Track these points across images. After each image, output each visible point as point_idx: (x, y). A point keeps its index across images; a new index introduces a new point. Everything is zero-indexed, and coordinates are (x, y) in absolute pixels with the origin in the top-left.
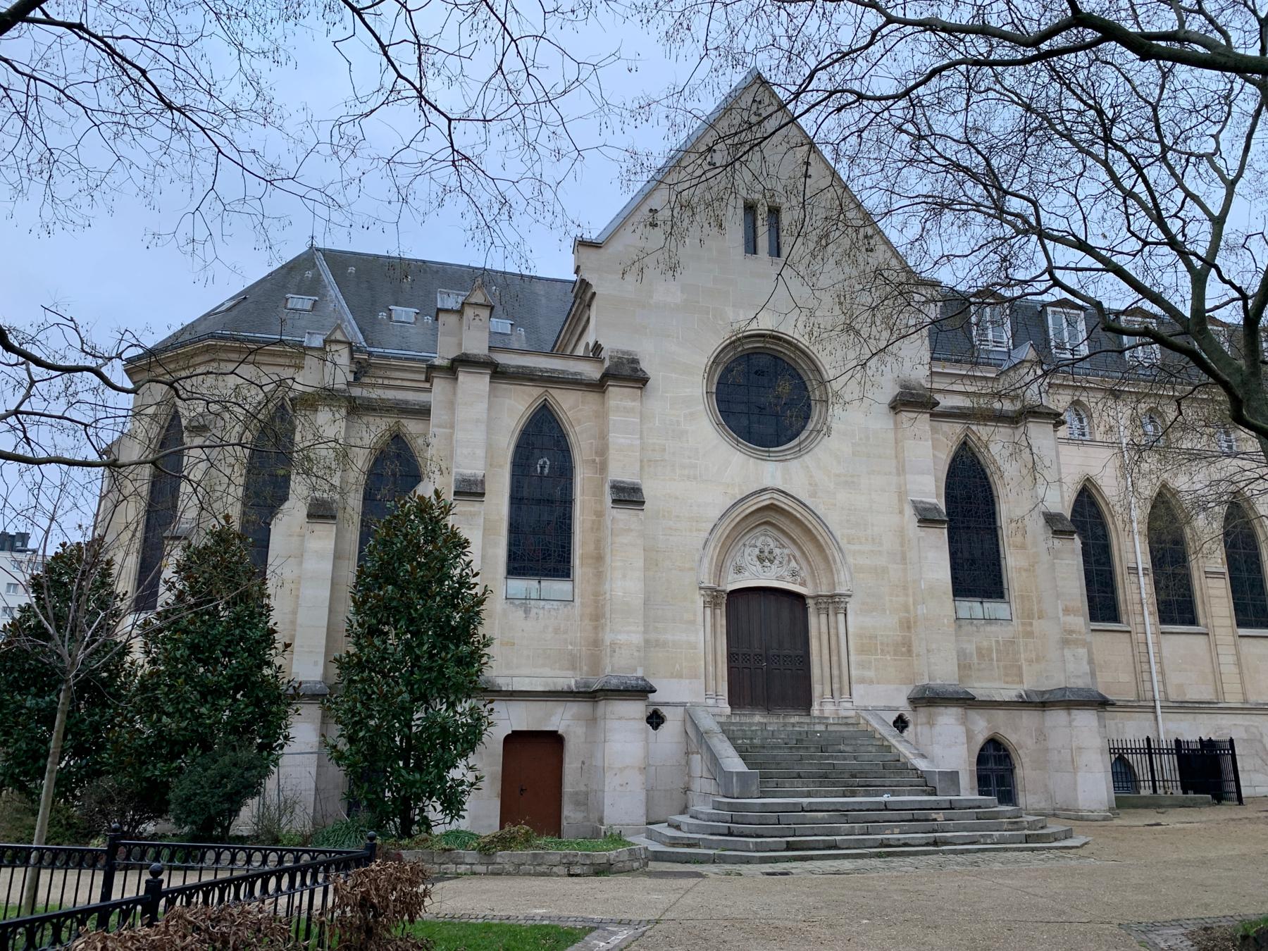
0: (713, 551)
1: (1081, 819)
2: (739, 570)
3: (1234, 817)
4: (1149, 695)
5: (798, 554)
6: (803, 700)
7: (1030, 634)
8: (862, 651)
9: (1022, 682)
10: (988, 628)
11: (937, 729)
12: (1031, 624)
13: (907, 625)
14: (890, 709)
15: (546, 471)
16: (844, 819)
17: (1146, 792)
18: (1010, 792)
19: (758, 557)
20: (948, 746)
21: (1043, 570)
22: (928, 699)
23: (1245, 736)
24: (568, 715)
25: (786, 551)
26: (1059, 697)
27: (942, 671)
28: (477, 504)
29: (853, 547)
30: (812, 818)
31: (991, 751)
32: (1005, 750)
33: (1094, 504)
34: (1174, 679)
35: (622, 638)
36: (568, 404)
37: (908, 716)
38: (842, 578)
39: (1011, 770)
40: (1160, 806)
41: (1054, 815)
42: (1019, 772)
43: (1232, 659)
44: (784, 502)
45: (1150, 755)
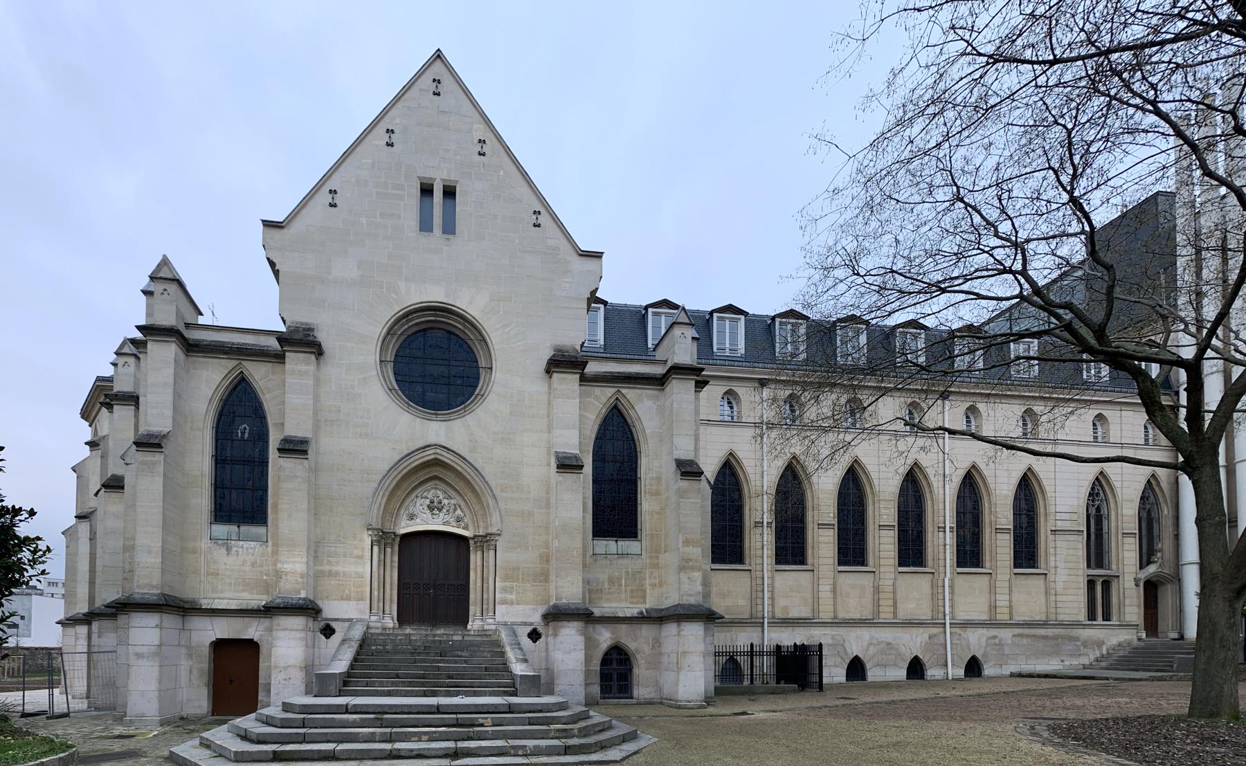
0: (381, 500)
1: (679, 707)
2: (412, 517)
3: (815, 704)
4: (760, 615)
5: (462, 504)
6: (462, 618)
7: (656, 566)
8: (506, 578)
9: (645, 602)
10: (620, 561)
11: (560, 638)
12: (657, 558)
13: (546, 559)
14: (525, 624)
15: (246, 435)
16: (378, 723)
17: (746, 682)
18: (626, 686)
19: (429, 507)
20: (570, 653)
21: (674, 513)
22: (556, 615)
23: (831, 642)
24: (261, 628)
25: (453, 502)
26: (672, 612)
27: (569, 590)
28: (157, 455)
29: (504, 495)
30: (341, 721)
31: (615, 656)
32: (626, 654)
33: (734, 474)
34: (781, 602)
35: (288, 567)
36: (258, 373)
37: (540, 630)
38: (494, 521)
39: (631, 670)
40: (754, 693)
41: (661, 703)
42: (636, 671)
43: (828, 588)
44: (447, 457)
45: (752, 656)
